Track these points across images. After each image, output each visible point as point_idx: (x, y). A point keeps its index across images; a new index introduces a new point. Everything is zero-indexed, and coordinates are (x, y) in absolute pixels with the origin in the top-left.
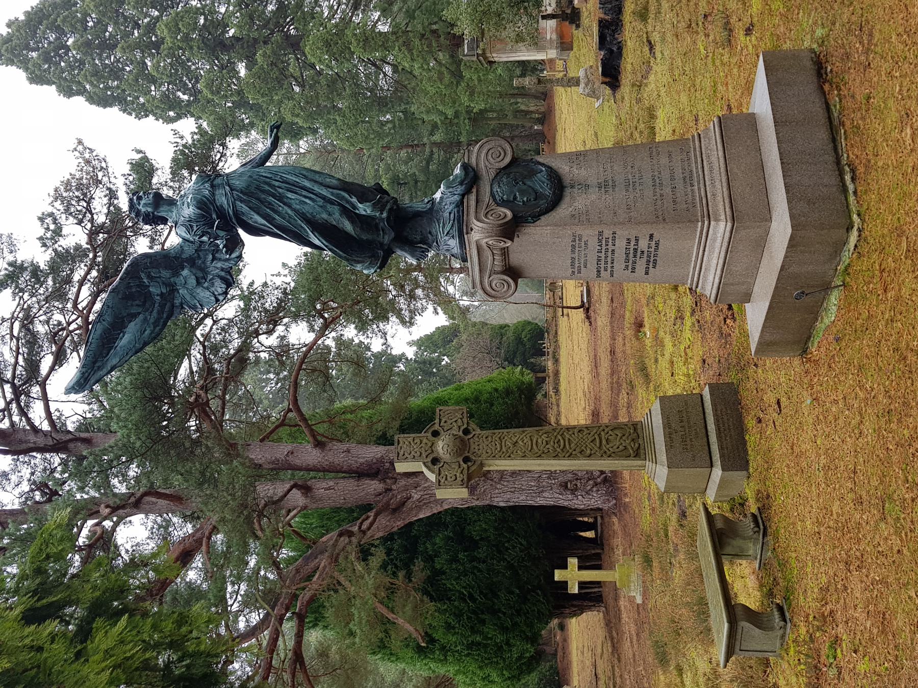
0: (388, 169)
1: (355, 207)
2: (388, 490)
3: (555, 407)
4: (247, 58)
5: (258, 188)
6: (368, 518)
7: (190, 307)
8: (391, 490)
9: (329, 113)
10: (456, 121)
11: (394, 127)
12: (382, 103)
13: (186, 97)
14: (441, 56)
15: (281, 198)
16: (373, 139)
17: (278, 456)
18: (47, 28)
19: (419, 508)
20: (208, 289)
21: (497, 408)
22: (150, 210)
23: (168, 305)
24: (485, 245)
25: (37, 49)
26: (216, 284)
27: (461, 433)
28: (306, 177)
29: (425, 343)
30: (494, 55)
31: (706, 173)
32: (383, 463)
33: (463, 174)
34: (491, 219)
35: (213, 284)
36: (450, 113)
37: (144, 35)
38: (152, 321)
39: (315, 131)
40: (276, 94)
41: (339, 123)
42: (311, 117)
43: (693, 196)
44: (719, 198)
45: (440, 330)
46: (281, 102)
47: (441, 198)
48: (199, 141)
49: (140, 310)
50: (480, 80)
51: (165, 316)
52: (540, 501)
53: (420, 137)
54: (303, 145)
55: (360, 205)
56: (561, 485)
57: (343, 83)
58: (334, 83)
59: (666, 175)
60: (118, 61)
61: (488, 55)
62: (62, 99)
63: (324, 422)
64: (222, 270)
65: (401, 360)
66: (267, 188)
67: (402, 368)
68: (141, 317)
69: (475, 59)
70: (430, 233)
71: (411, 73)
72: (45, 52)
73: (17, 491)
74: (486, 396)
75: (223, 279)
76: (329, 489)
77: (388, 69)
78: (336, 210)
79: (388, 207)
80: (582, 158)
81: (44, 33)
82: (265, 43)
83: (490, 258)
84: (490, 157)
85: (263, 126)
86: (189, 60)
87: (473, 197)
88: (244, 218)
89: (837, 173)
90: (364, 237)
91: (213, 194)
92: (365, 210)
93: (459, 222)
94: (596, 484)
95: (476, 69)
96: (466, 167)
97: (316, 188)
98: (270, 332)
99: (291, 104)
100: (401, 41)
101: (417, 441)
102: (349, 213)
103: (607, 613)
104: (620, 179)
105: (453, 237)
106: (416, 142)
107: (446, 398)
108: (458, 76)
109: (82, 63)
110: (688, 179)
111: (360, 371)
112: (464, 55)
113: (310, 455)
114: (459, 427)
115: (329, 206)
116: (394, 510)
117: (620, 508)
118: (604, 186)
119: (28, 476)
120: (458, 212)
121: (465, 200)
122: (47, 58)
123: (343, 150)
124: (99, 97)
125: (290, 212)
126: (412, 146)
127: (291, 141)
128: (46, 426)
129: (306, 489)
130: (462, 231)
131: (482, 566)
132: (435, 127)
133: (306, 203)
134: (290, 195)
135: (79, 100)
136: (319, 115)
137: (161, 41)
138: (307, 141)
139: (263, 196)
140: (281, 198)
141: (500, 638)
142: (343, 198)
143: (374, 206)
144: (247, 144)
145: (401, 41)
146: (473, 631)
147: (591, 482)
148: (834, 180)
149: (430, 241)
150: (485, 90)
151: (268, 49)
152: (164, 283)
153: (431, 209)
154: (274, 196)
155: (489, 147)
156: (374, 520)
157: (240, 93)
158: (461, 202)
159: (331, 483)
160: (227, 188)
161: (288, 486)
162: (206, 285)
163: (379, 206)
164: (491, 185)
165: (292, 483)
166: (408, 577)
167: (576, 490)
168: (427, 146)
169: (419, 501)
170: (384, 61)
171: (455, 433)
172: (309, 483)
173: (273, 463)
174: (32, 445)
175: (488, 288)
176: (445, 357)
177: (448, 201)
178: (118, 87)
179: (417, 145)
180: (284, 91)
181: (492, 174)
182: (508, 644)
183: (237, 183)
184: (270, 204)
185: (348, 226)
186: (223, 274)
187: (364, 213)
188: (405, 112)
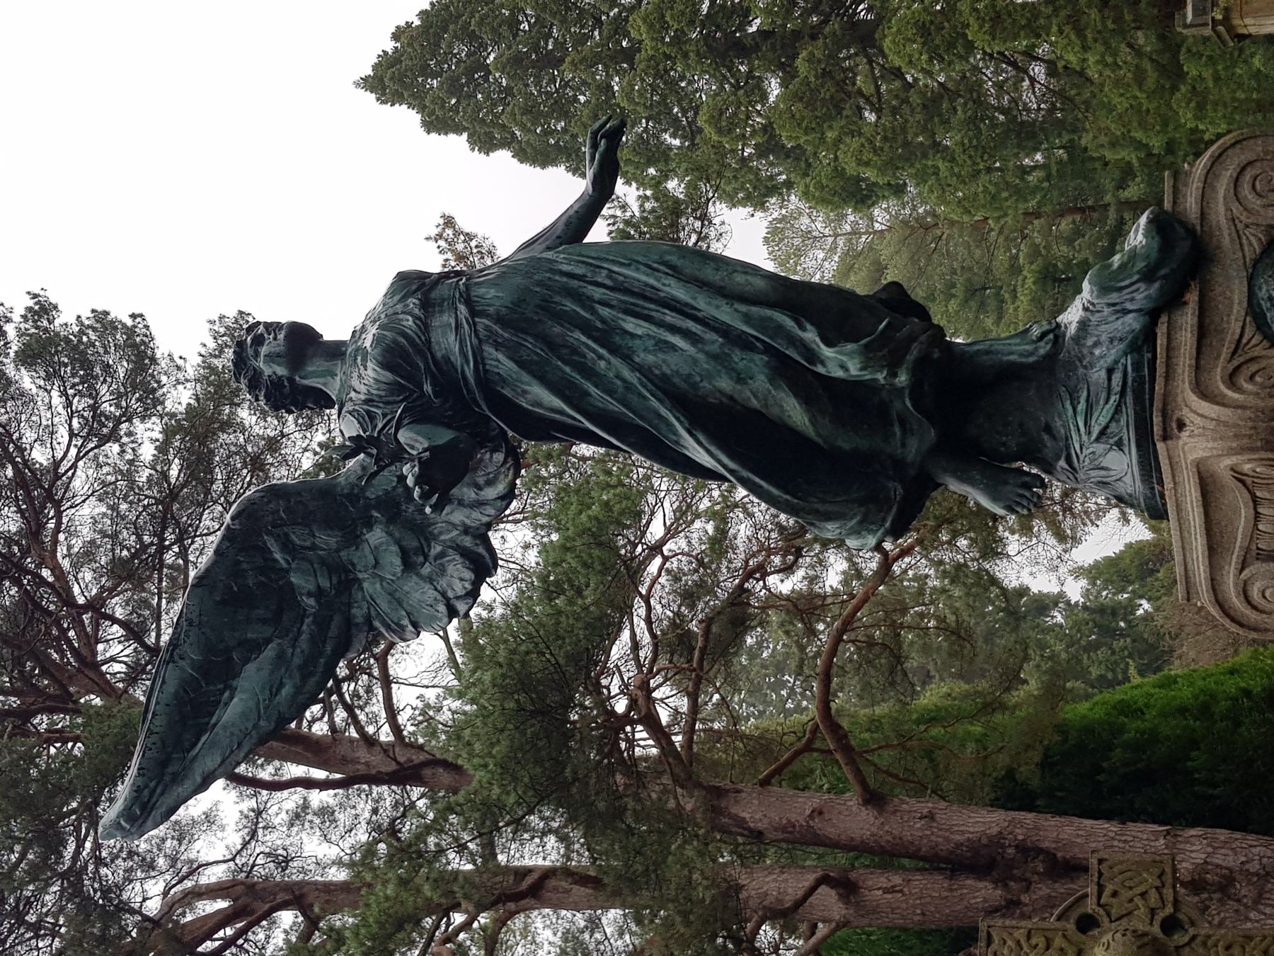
0: (1035, 252)
1: (813, 357)
4: (782, 66)
5: (547, 308)
7: (388, 627)
9: (925, 156)
10: (1170, 159)
11: (1048, 178)
12: (1025, 134)
13: (677, 142)
14: (1140, 38)
15: (608, 337)
16: (1006, 199)
18: (455, 36)
20: (430, 580)
22: (281, 371)
23: (337, 620)
24: (1227, 478)
25: (424, 74)
26: (450, 569)
27: (1156, 929)
28: (675, 272)
29: (1107, 572)
30: (1248, 21)
32: (1003, 846)
33: (1155, 245)
34: (1248, 392)
35: (442, 570)
36: (1156, 144)
37: (609, 38)
38: (297, 661)
39: (899, 190)
40: (831, 127)
41: (944, 172)
42: (891, 165)
45: (1135, 550)
46: (838, 141)
47: (1083, 325)
48: (653, 211)
49: (268, 631)
50: (1217, 79)
51: (329, 649)
53: (1099, 191)
54: (881, 215)
55: (827, 352)
57: (952, 101)
58: (935, 104)
60: (567, 84)
61: (1236, 22)
62: (478, 156)
63: (888, 746)
64: (466, 530)
65: (1056, 604)
66: (570, 305)
67: (1059, 619)
68: (270, 652)
69: (1207, 31)
70: (1048, 429)
71: (1081, 73)
72: (451, 78)
73: (347, 844)
74: (1224, 704)
75: (465, 553)
77: (1038, 70)
78: (756, 364)
79: (910, 357)
81: (450, 46)
82: (814, 37)
83: (1245, 513)
84: (1246, 190)
85: (807, 186)
86: (682, 78)
87: (1187, 319)
88: (507, 392)
90: (845, 442)
91: (424, 326)
92: (843, 367)
93: (1138, 399)
95: (1210, 58)
96: (1164, 226)
97: (703, 304)
98: (787, 570)
99: (855, 143)
100: (1063, 13)
101: (1038, 940)
102: (796, 373)
105: (1119, 445)
106: (1090, 203)
107: (1140, 704)
108: (1173, 73)
109: (508, 91)
111: (962, 647)
112: (1186, 26)
113: (854, 819)
114: (1153, 912)
115: (737, 355)
119: (367, 815)
120: (1137, 367)
121: (1161, 330)
122: (453, 87)
123: (952, 223)
124: (534, 148)
125: (627, 373)
126: (1082, 210)
127: (855, 210)
128: (386, 735)
129: (847, 888)
130: (1149, 426)
132: (1127, 173)
133: (673, 348)
134: (631, 324)
135: (503, 157)
136: (907, 160)
137: (636, 47)
138: (886, 210)
139: (557, 329)
140: (608, 337)
142: (779, 330)
143: (869, 356)
144: (783, 219)
145: (1063, 13)
149: (1048, 453)
150: (1228, 98)
151: (817, 49)
152: (323, 562)
153: (1051, 357)
154: (587, 329)
155: (1250, 156)
157: (767, 128)
159: (897, 880)
160: (462, 308)
161: (810, 878)
162: (426, 570)
163: (885, 351)
164: (1251, 279)
165: (819, 873)
168: (1112, 210)
170: (1031, 56)
171: (1141, 928)
172: (853, 875)
173: (784, 829)
174: (362, 769)
175: (1236, 602)
176: (1144, 602)
177: (1105, 332)
178: (565, 130)
179: (1092, 208)
180: (843, 122)
181: (1254, 242)
183: (489, 295)
184: (575, 351)
185: (795, 413)
186: (467, 542)
187: (840, 374)
188: (1070, 147)
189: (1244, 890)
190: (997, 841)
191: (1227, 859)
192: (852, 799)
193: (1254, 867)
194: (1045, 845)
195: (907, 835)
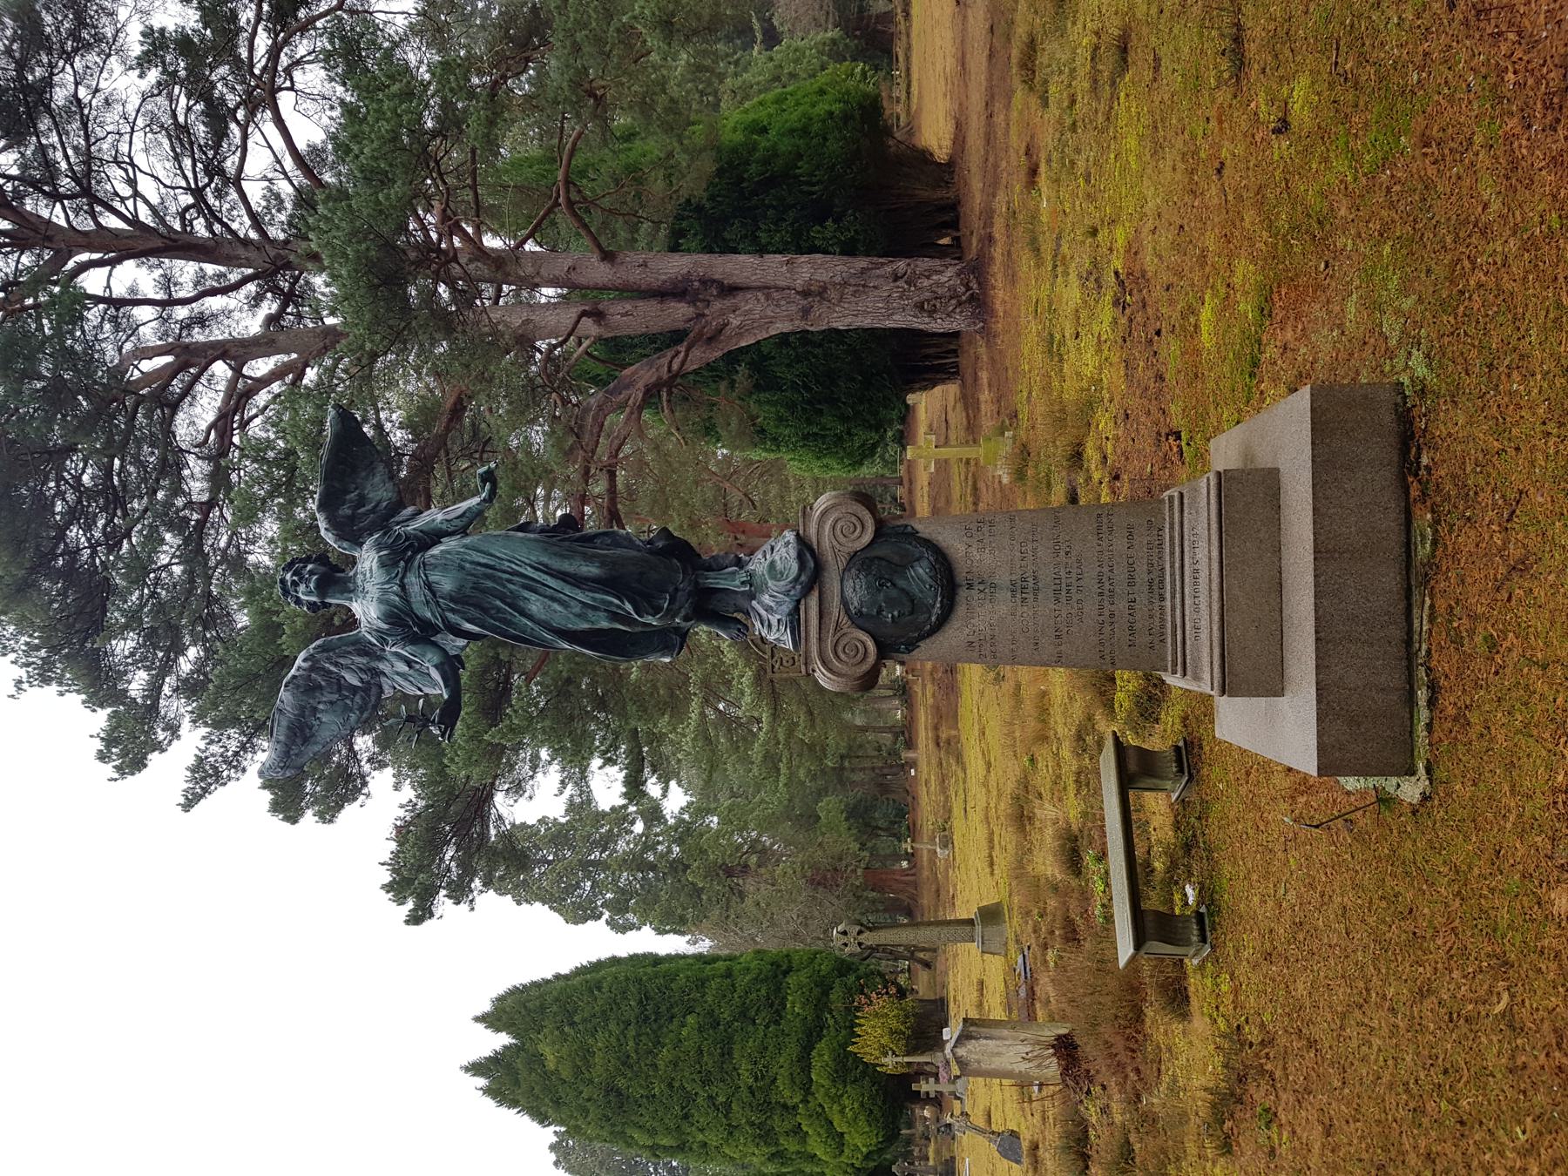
2: (701, 315)
3: (904, 38)
6: (678, 353)
8: (703, 315)
17: (557, 273)
19: (740, 335)
21: (833, 146)
31: (1187, 580)
43: (1162, 620)
44: (1204, 636)
52: (889, 324)
56: (916, 306)
59: (1121, 574)
66: (490, 584)
76: (626, 314)
80: (986, 529)
89: (1404, 663)
94: (960, 304)
103: (963, 386)
104: (1046, 575)
110: (1155, 586)
115: (590, 613)
116: (710, 340)
117: (988, 334)
118: (1022, 588)
121: (802, 608)
129: (598, 315)
131: (817, 351)
141: (840, 428)
146: (809, 422)
147: (954, 302)
148: (1397, 680)
156: (687, 356)
158: (797, 609)
159: (628, 307)
166: (732, 384)
167: (935, 311)
169: (739, 327)
172: (601, 307)
182: (849, 433)
189: (833, 294)
190: (687, 278)
191: (823, 276)
192: (595, 258)
193: (838, 279)
194: (716, 277)
195: (632, 279)
